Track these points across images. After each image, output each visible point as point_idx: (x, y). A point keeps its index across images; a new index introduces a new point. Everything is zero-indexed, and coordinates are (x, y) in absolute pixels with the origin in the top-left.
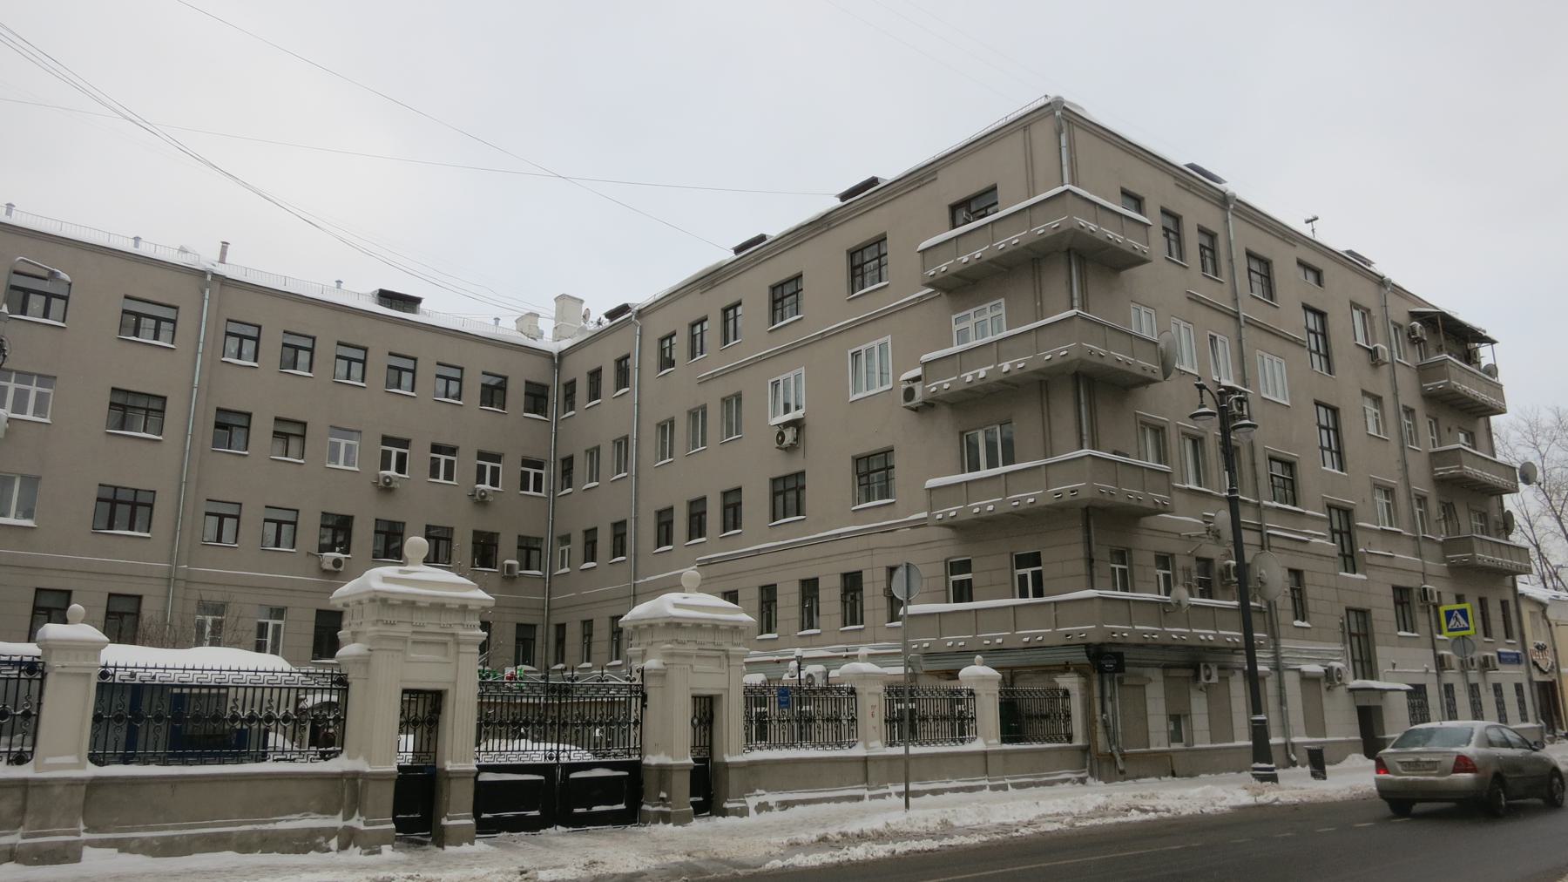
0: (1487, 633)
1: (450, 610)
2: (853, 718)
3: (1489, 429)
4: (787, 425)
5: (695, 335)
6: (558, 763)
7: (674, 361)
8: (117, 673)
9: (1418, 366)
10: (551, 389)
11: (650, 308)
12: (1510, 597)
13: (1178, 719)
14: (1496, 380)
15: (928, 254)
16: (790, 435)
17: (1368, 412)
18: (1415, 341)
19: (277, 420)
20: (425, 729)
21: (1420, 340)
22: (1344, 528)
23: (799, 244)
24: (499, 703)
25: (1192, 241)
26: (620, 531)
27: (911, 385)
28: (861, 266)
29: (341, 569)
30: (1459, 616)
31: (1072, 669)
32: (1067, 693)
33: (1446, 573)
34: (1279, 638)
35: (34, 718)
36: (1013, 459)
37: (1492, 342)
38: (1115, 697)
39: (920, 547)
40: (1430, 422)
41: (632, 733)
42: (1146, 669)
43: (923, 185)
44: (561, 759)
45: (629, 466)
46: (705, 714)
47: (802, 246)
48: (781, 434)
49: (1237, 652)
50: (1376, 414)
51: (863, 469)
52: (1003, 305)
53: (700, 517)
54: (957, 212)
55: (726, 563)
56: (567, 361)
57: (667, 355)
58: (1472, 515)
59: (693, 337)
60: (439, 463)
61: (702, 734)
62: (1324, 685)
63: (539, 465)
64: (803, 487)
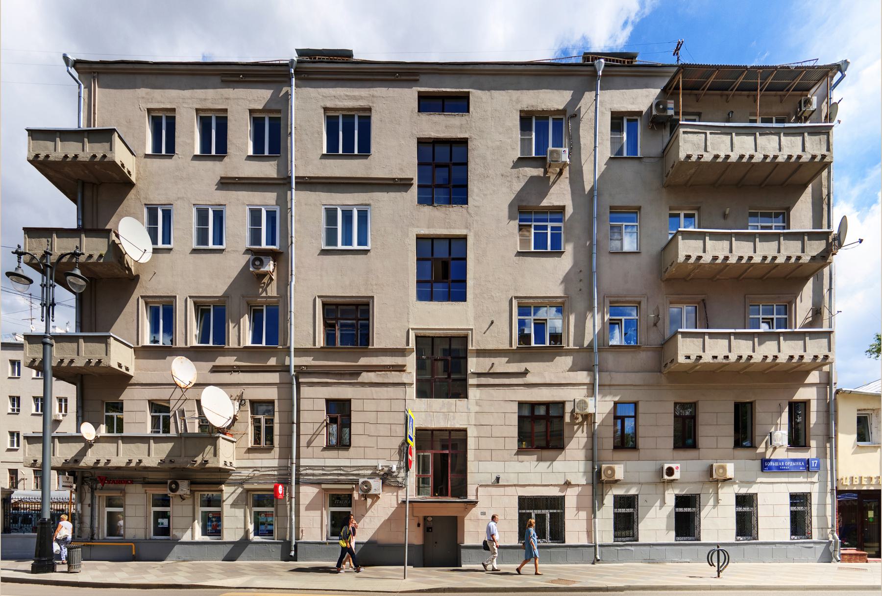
6: (76, 262)
19: (34, 134)
24: (540, 418)
36: (614, 131)
45: (85, 148)
55: (507, 314)
58: (835, 229)
60: (341, 342)
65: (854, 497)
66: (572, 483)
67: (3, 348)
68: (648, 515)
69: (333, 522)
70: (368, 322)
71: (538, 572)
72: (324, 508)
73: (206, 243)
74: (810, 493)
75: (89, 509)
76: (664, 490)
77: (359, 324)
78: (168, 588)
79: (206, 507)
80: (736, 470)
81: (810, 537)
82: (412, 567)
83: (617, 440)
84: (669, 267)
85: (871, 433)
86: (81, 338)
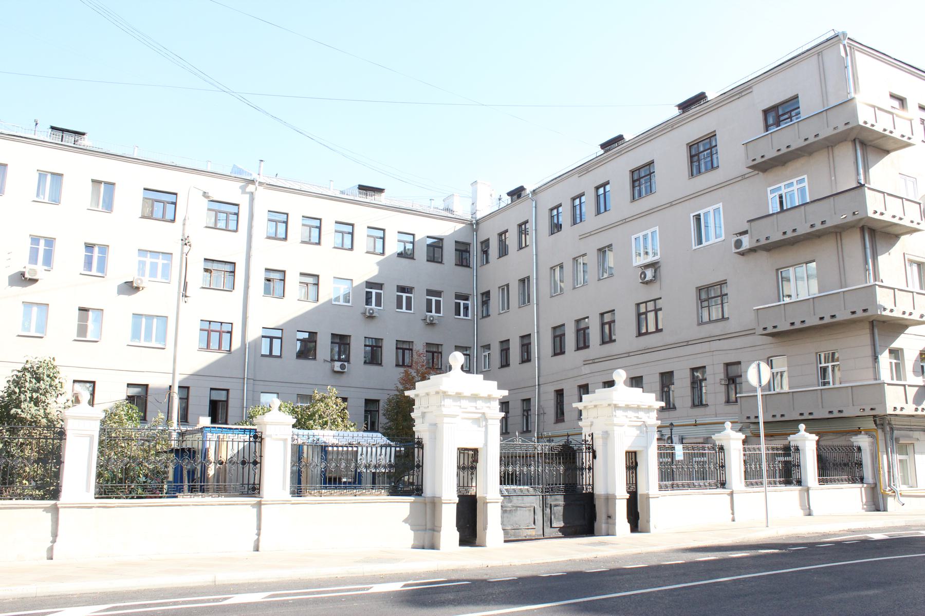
1: (465, 398)
4: (647, 266)
7: (561, 225)
8: (248, 438)
10: (471, 246)
11: (541, 188)
15: (750, 145)
16: (649, 274)
19: (267, 270)
20: (470, 473)
26: (526, 341)
27: (739, 238)
28: (698, 155)
29: (346, 370)
31: (863, 432)
32: (859, 449)
35: (421, 468)
39: (750, 349)
41: (588, 476)
42: (915, 432)
43: (742, 96)
44: (588, 490)
46: (632, 463)
48: (643, 273)
51: (704, 296)
52: (806, 180)
53: (584, 332)
54: (768, 115)
56: (481, 226)
57: (556, 221)
59: (574, 207)
61: (631, 476)
63: (466, 298)
66: (50, 174)
67: (478, 541)
68: (907, 331)
71: (903, 387)
73: (156, 276)
76: (874, 345)
78: (803, 328)
79: (874, 511)
81: (764, 396)
84: (58, 405)
85: (719, 340)
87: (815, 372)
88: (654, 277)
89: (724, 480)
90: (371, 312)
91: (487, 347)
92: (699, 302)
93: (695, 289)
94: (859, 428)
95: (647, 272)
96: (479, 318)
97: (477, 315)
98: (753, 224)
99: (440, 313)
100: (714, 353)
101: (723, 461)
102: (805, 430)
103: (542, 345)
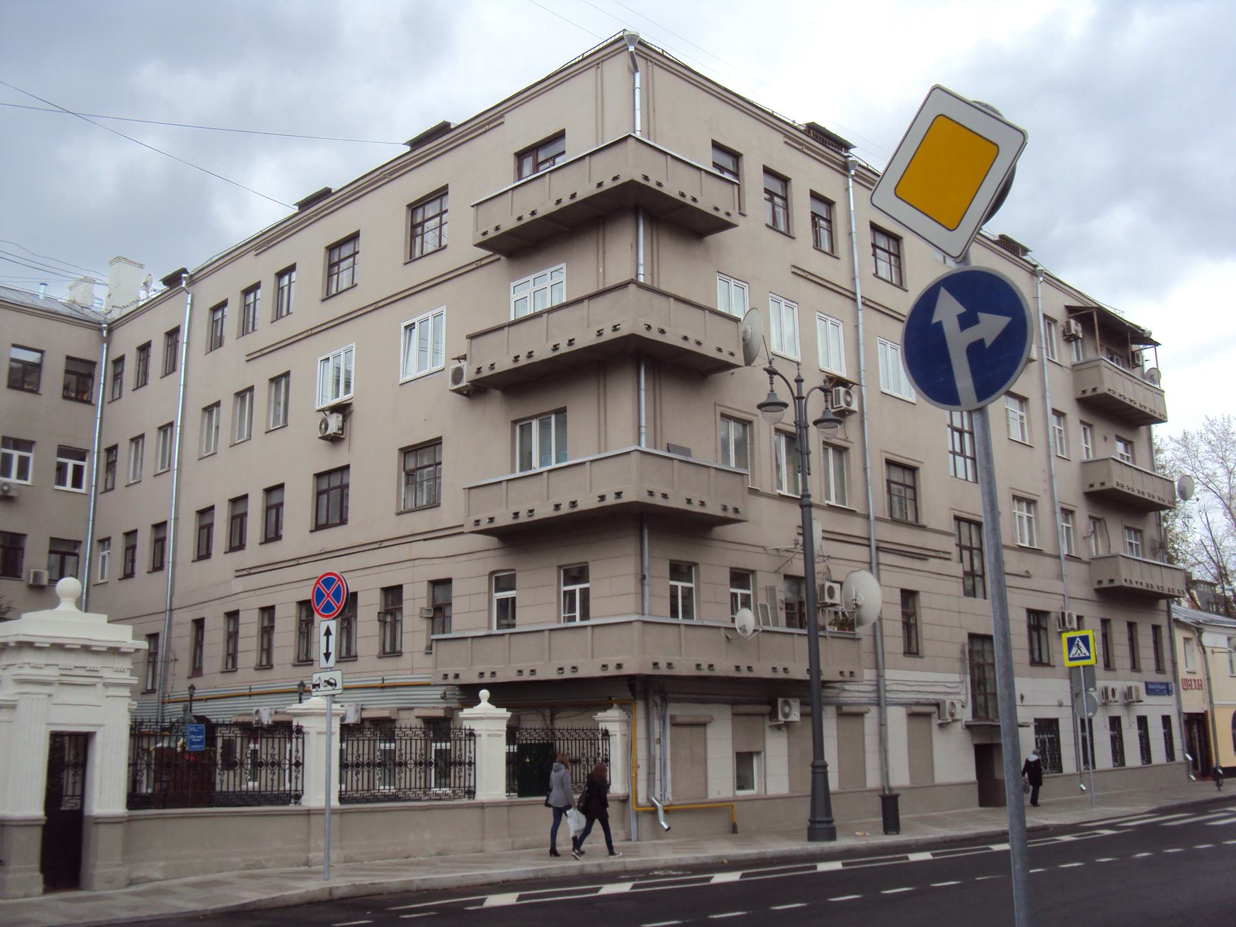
0: (1108, 666)
2: (606, 759)
3: (1150, 439)
5: (249, 305)
9: (1074, 366)
10: (97, 366)
12: (1162, 620)
13: (744, 761)
14: (1157, 386)
17: (1011, 414)
18: (1069, 338)
21: (1076, 338)
22: (975, 544)
23: (359, 197)
25: (802, 207)
30: (1081, 644)
32: (606, 734)
33: (1092, 595)
34: (884, 668)
37: (1156, 344)
38: (665, 739)
40: (1085, 429)
47: (362, 200)
48: (325, 423)
49: (828, 685)
50: (1021, 417)
52: (564, 270)
59: (246, 306)
61: (355, 778)
62: (935, 721)
64: (347, 486)
65: (213, 781)
69: (551, 752)
70: (67, 739)
72: (560, 162)
74: (731, 568)
75: (557, 160)
77: (501, 632)
80: (1115, 448)
82: (505, 709)
83: (891, 247)
85: (425, 540)
86: (643, 805)
87: (554, 599)
88: (342, 429)
89: (472, 784)
90: (6, 488)
91: (105, 542)
92: (403, 474)
93: (396, 452)
94: (610, 698)
95: (329, 420)
96: (99, 491)
97: (96, 487)
98: (475, 342)
99: (26, 479)
100: (417, 562)
101: (472, 755)
102: (490, 701)
103: (183, 539)
